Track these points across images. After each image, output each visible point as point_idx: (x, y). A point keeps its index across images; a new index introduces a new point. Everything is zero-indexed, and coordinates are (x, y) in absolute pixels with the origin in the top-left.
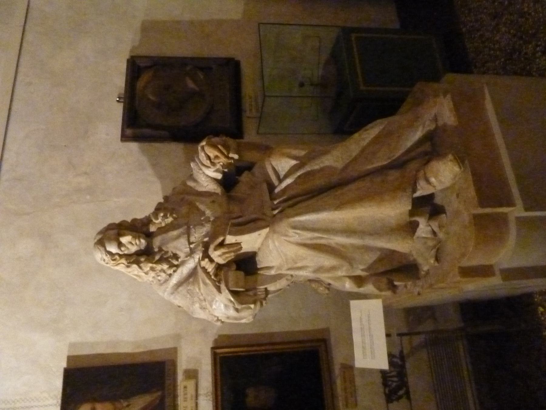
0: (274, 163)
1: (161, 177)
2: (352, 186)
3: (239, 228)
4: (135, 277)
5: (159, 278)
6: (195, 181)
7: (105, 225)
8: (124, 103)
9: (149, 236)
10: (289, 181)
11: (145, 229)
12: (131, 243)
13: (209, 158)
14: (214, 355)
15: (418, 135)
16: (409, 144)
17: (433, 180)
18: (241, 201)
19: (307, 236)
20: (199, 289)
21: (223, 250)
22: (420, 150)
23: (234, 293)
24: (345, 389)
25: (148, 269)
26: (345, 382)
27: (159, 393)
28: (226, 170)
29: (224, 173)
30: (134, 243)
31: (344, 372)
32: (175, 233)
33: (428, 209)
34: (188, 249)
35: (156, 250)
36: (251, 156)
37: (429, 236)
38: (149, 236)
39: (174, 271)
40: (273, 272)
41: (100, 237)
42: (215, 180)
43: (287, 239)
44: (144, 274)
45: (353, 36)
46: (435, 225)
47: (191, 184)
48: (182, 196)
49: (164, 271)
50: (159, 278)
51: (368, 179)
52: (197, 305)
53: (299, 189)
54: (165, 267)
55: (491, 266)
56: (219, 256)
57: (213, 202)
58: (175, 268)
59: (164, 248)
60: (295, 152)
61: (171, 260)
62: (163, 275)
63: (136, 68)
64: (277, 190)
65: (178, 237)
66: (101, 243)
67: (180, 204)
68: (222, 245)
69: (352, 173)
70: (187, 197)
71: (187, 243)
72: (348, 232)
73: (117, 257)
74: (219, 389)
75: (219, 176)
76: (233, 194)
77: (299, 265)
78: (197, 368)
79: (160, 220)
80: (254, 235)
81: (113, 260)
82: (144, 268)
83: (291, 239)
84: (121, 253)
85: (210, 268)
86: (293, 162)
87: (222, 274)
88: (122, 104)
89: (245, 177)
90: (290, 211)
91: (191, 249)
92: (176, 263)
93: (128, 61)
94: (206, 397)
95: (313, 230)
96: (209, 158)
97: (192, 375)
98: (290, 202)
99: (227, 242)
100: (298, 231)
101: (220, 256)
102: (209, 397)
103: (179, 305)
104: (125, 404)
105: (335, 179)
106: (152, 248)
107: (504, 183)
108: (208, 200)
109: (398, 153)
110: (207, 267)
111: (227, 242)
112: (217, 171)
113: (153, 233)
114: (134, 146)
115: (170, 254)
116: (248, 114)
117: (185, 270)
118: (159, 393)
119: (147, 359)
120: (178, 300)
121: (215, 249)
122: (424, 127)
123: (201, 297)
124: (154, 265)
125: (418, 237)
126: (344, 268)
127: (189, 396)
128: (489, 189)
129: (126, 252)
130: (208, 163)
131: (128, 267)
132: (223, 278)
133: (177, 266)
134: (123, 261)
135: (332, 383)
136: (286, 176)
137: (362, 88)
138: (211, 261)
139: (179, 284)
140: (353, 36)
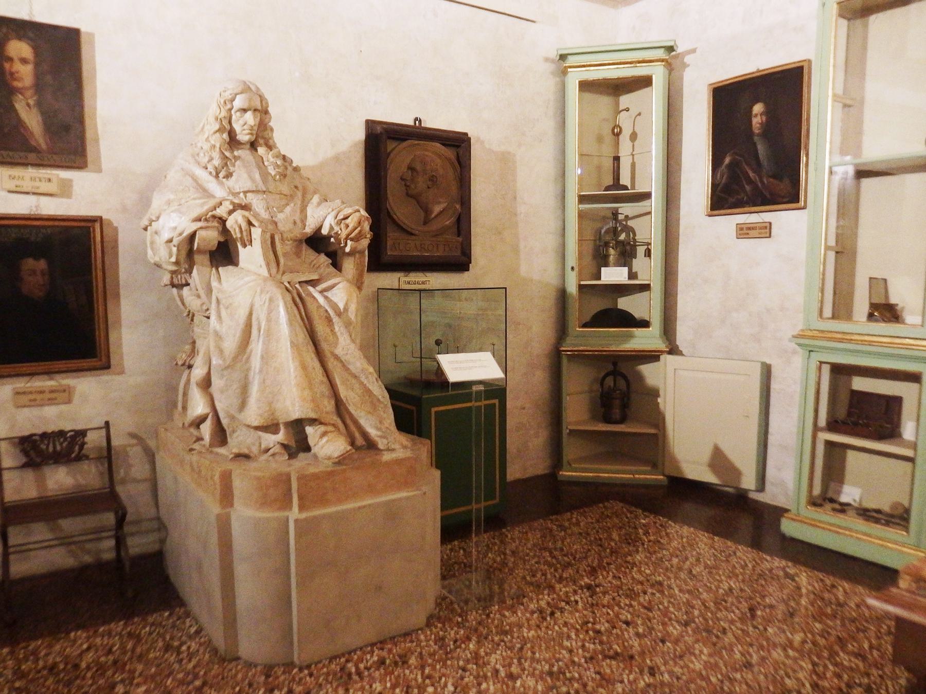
0: (340, 286)
1: (322, 165)
2: (317, 364)
3: (269, 242)
4: (201, 125)
5: (202, 155)
6: (319, 204)
7: (267, 96)
8: (414, 127)
9: (253, 145)
10: (321, 300)
11: (261, 141)
12: (244, 126)
13: (346, 218)
14: (93, 220)
15: (373, 432)
16: (362, 422)
17: (325, 439)
18: (298, 254)
19: (261, 314)
20: (194, 199)
21: (244, 225)
22: (357, 435)
23: (192, 236)
24: (42, 392)
25: (213, 142)
26: (52, 392)
27: (44, 146)
28: (332, 240)
29: (328, 237)
30: (245, 127)
31: (64, 391)
32: (257, 176)
33: (293, 444)
34: (238, 190)
35: (236, 153)
36: (349, 265)
37: (263, 446)
38: (253, 145)
39: (211, 173)
40: (214, 284)
41: (253, 88)
42: (320, 228)
43: (258, 294)
44: (209, 139)
45: (496, 401)
46: (278, 449)
47: (316, 199)
48: (300, 188)
49: (211, 159)
50: (202, 155)
51: (325, 379)
52: (172, 197)
53: (311, 307)
54: (217, 162)
55: (232, 505)
56: (235, 221)
57: (295, 223)
58: (214, 173)
59: (238, 163)
60: (353, 307)
61: (223, 171)
62: (206, 159)
63: (457, 144)
64: (311, 289)
65: (253, 180)
66: (246, 88)
67: (292, 181)
68: (250, 224)
69: (332, 364)
70: (299, 194)
71: (246, 189)
72: (266, 358)
73: (229, 106)
74: (51, 223)
75: (325, 231)
76: (304, 246)
77: (224, 313)
78: (74, 197)
79: (272, 160)
80: (261, 260)
81: (225, 103)
82: (214, 137)
83: (257, 298)
84: (233, 112)
85: (221, 212)
86: (341, 306)
87: (216, 224)
88: (412, 123)
89: (323, 259)
90: (288, 297)
91: (239, 193)
92: (221, 175)
93: (466, 134)
94: (36, 207)
95: (269, 320)
96: (346, 218)
97: (65, 190)
98: (298, 299)
99: (253, 229)
100: (267, 304)
101: (236, 222)
102: (34, 209)
103: (168, 177)
104: (31, 102)
105: (324, 346)
106: (238, 149)
107: (323, 501)
108: (297, 217)
109: (352, 409)
110: (222, 207)
111: (253, 229)
112: (331, 228)
113: (256, 150)
114: (360, 135)
115: (232, 169)
116: (403, 279)
117: (213, 186)
118: (44, 146)
119: (89, 135)
120: (173, 176)
121: (244, 216)
122: (381, 437)
123: (183, 201)
124: (218, 149)
125: (260, 438)
126: (221, 362)
127: (37, 184)
128: (315, 490)
129: (234, 117)
130: (341, 216)
131: (217, 119)
132: (210, 224)
133: (217, 176)
134: (224, 113)
135: (49, 373)
136: (326, 298)
137: (434, 410)
138: (230, 212)
139: (195, 179)
140: (496, 401)
